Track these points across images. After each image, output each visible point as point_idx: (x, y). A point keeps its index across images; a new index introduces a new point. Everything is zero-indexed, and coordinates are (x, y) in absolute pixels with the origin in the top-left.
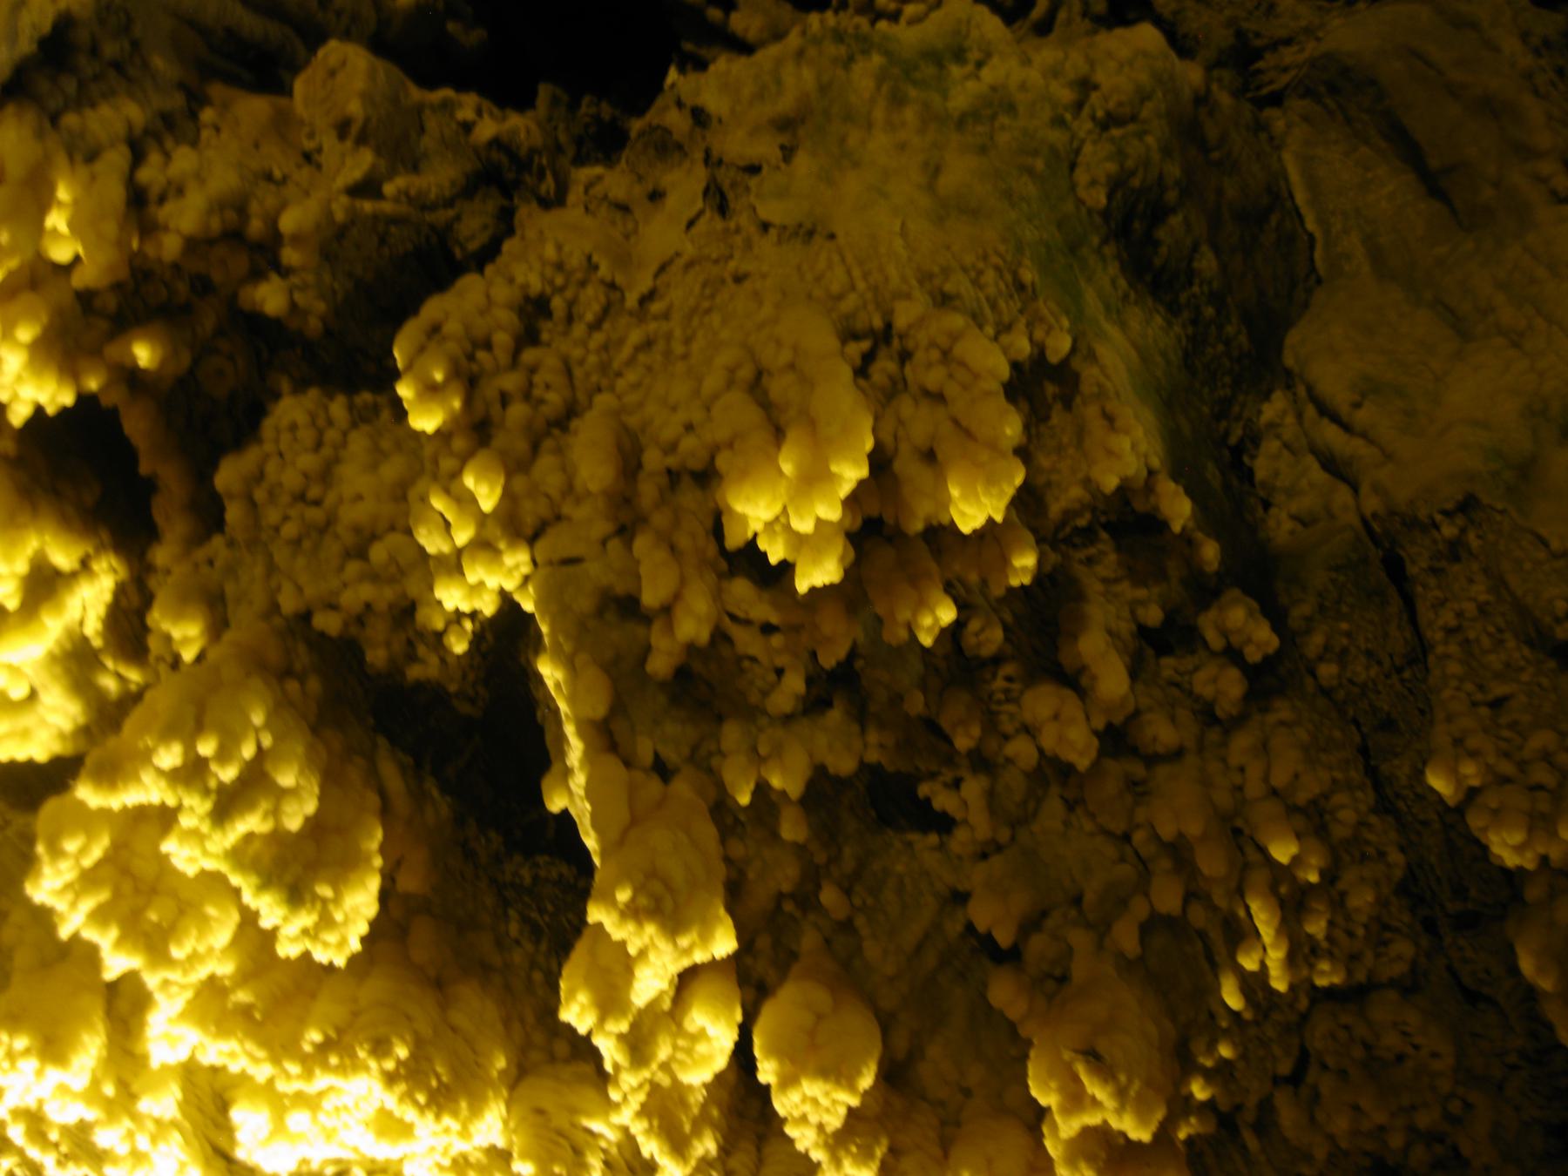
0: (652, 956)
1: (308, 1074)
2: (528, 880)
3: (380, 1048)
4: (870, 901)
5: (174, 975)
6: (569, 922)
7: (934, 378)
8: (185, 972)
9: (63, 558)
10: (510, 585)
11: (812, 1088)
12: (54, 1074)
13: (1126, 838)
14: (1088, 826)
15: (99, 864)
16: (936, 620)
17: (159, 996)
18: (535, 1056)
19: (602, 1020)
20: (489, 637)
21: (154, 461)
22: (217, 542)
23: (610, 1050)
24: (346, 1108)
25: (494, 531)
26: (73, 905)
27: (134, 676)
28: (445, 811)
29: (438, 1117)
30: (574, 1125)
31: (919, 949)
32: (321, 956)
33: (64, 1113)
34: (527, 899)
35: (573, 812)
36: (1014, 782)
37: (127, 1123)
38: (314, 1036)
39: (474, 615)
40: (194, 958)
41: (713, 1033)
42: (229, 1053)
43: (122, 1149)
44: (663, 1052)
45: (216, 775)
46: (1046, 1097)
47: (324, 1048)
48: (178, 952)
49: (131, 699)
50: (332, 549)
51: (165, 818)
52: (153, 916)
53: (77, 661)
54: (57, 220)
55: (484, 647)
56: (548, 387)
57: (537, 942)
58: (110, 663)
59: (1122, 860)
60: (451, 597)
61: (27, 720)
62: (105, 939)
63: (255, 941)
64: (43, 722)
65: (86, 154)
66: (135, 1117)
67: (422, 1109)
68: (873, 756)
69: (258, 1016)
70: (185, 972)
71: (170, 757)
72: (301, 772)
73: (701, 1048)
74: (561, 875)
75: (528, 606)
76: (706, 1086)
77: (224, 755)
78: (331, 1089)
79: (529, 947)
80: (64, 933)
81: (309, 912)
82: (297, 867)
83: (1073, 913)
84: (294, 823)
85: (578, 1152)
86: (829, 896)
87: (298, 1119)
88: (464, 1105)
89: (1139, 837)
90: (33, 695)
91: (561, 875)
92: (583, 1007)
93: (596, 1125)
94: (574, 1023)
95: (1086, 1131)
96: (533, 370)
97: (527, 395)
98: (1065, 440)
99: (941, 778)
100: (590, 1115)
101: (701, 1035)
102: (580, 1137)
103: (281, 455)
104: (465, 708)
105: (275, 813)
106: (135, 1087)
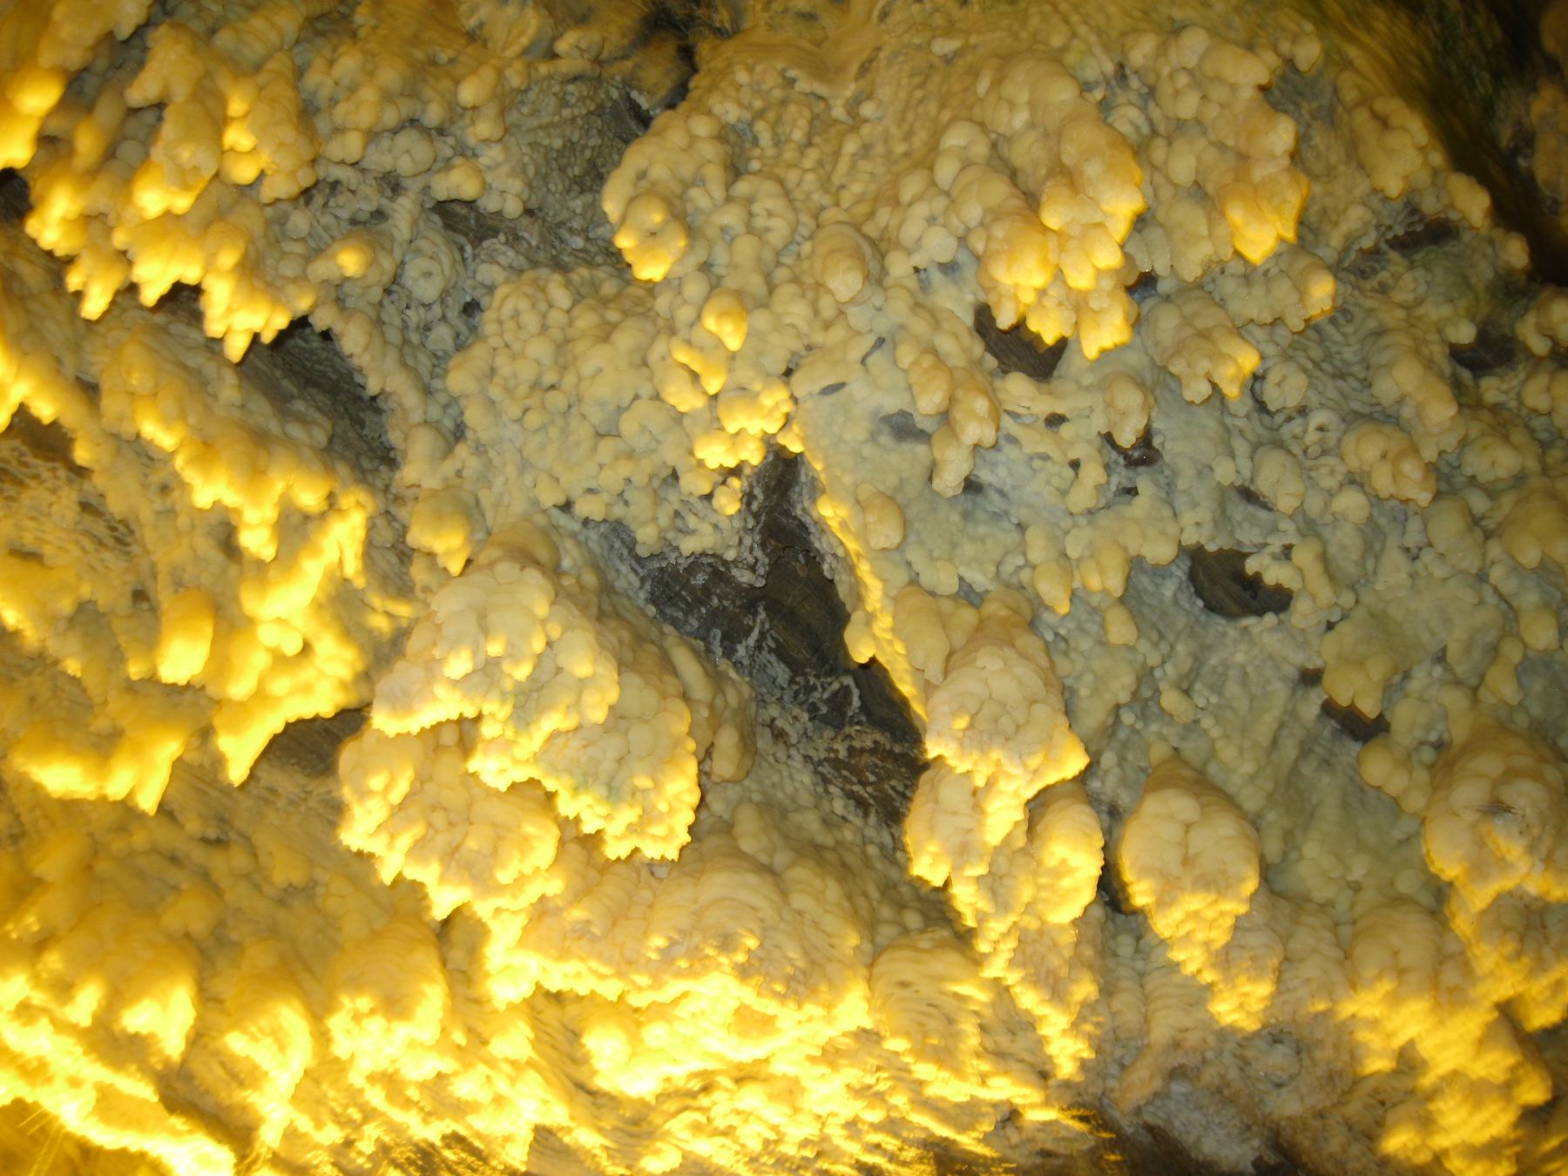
0: (1003, 785)
1: (657, 984)
2: (843, 754)
3: (727, 943)
4: (1214, 699)
5: (504, 901)
6: (893, 788)
7: (1187, 106)
8: (515, 897)
9: (310, 498)
10: (772, 428)
11: (1194, 902)
12: (402, 1029)
13: (1482, 577)
14: (1439, 571)
15: (408, 797)
16: (1240, 369)
17: (492, 925)
18: (887, 931)
19: (957, 867)
20: (758, 492)
21: (380, 374)
22: (462, 450)
23: (967, 899)
24: (703, 1013)
25: (744, 374)
26: (391, 845)
27: (403, 610)
28: (746, 691)
29: (800, 1005)
30: (943, 993)
31: (1275, 742)
32: (652, 851)
33: (419, 1069)
34: (845, 773)
35: (881, 659)
36: (1346, 542)
37: (482, 1069)
38: (659, 941)
39: (736, 472)
40: (521, 880)
41: (1074, 860)
42: (573, 975)
43: (484, 1096)
44: (1026, 894)
45: (510, 676)
46: (1448, 866)
47: (667, 955)
48: (504, 876)
49: (401, 636)
50: (582, 432)
51: (464, 734)
52: (472, 843)
53: (342, 604)
54: (238, 137)
55: (755, 506)
56: (770, 214)
57: (866, 815)
58: (376, 601)
59: (1481, 602)
60: (715, 454)
61: (306, 674)
62: (427, 873)
63: (581, 845)
64: (322, 674)
65: (249, 70)
66: (491, 1062)
67: (782, 998)
68: (1191, 538)
69: (596, 930)
70: (515, 897)
71: (459, 665)
72: (595, 661)
73: (1066, 883)
74: (875, 742)
75: (795, 447)
76: (1075, 923)
77: (513, 655)
78: (685, 995)
79: (858, 822)
80: (387, 875)
81: (632, 806)
82: (610, 763)
83: (1438, 671)
84: (598, 715)
85: (950, 1021)
86: (1171, 700)
87: (654, 1033)
88: (823, 988)
89: (1496, 574)
90: (307, 649)
91: (875, 742)
92: (936, 856)
93: (964, 989)
94: (927, 877)
95: (1499, 899)
96: (749, 200)
97: (750, 230)
98: (1333, 159)
99: (1269, 549)
100: (955, 980)
101: (1062, 870)
102: (949, 1004)
103: (507, 346)
104: (744, 577)
105: (577, 705)
106: (481, 1028)
